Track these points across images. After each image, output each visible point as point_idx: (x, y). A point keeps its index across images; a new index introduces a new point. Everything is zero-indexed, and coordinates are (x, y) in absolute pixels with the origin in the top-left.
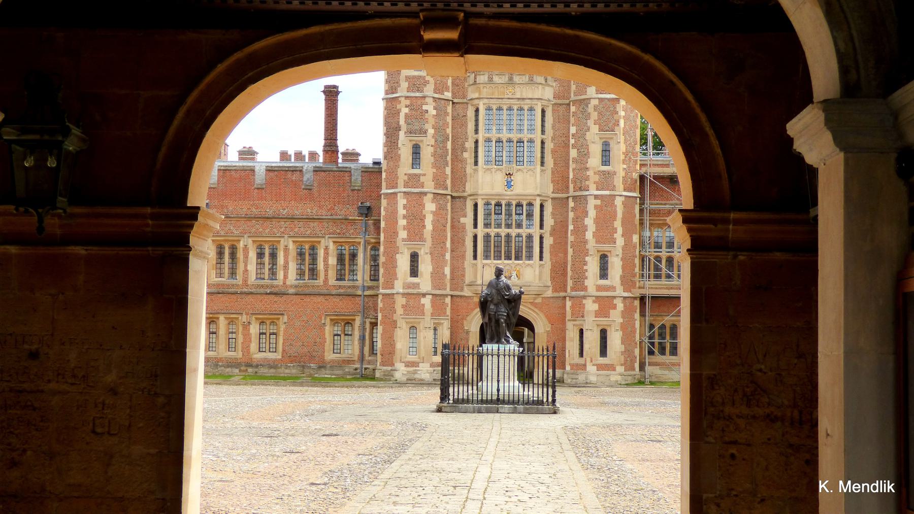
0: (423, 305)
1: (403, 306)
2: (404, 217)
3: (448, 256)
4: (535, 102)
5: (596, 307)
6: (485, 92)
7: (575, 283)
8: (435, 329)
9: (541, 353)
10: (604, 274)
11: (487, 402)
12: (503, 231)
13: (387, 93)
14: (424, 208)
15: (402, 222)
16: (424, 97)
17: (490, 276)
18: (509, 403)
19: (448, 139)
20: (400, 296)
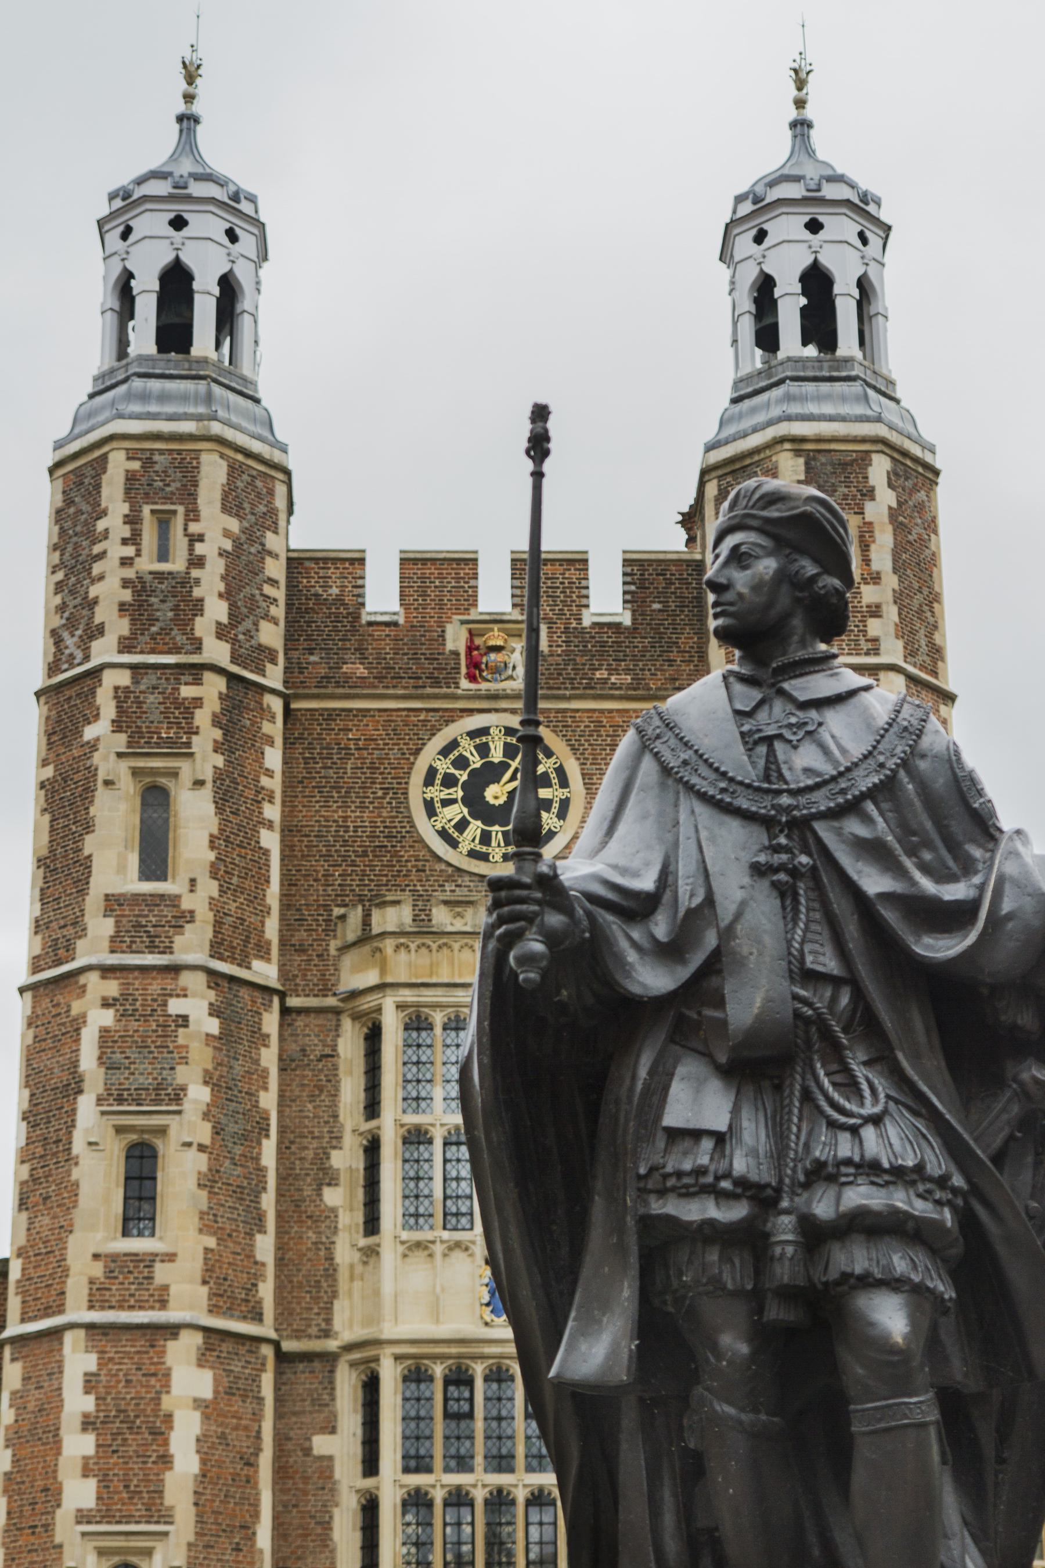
2: (87, 1424)
6: (403, 965)
12: (480, 1482)
13: (36, 966)
14: (166, 1387)
15: (78, 1445)
16: (175, 969)
19: (265, 1132)
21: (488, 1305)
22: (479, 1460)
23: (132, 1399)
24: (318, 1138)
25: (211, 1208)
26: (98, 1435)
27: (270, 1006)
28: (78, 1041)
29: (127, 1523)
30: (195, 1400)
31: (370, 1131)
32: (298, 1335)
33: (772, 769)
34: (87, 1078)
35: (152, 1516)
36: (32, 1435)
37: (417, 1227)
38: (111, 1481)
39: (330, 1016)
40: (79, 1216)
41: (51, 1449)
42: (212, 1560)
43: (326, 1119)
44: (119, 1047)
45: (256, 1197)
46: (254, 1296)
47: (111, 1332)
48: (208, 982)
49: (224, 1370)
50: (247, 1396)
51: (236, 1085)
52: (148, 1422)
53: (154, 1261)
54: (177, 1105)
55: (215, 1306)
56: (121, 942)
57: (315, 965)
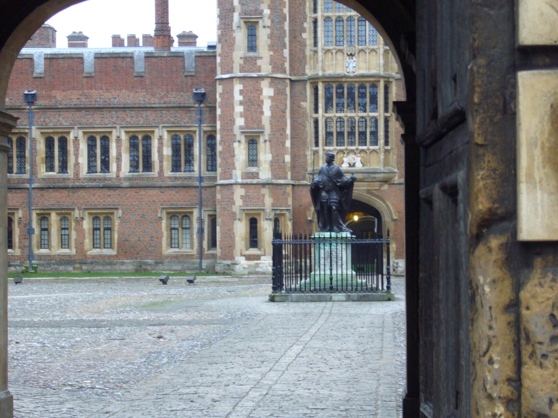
1: (242, 197)
2: (241, 103)
3: (288, 144)
15: (239, 109)
19: (285, 20)
32: (295, 75)
34: (236, 8)
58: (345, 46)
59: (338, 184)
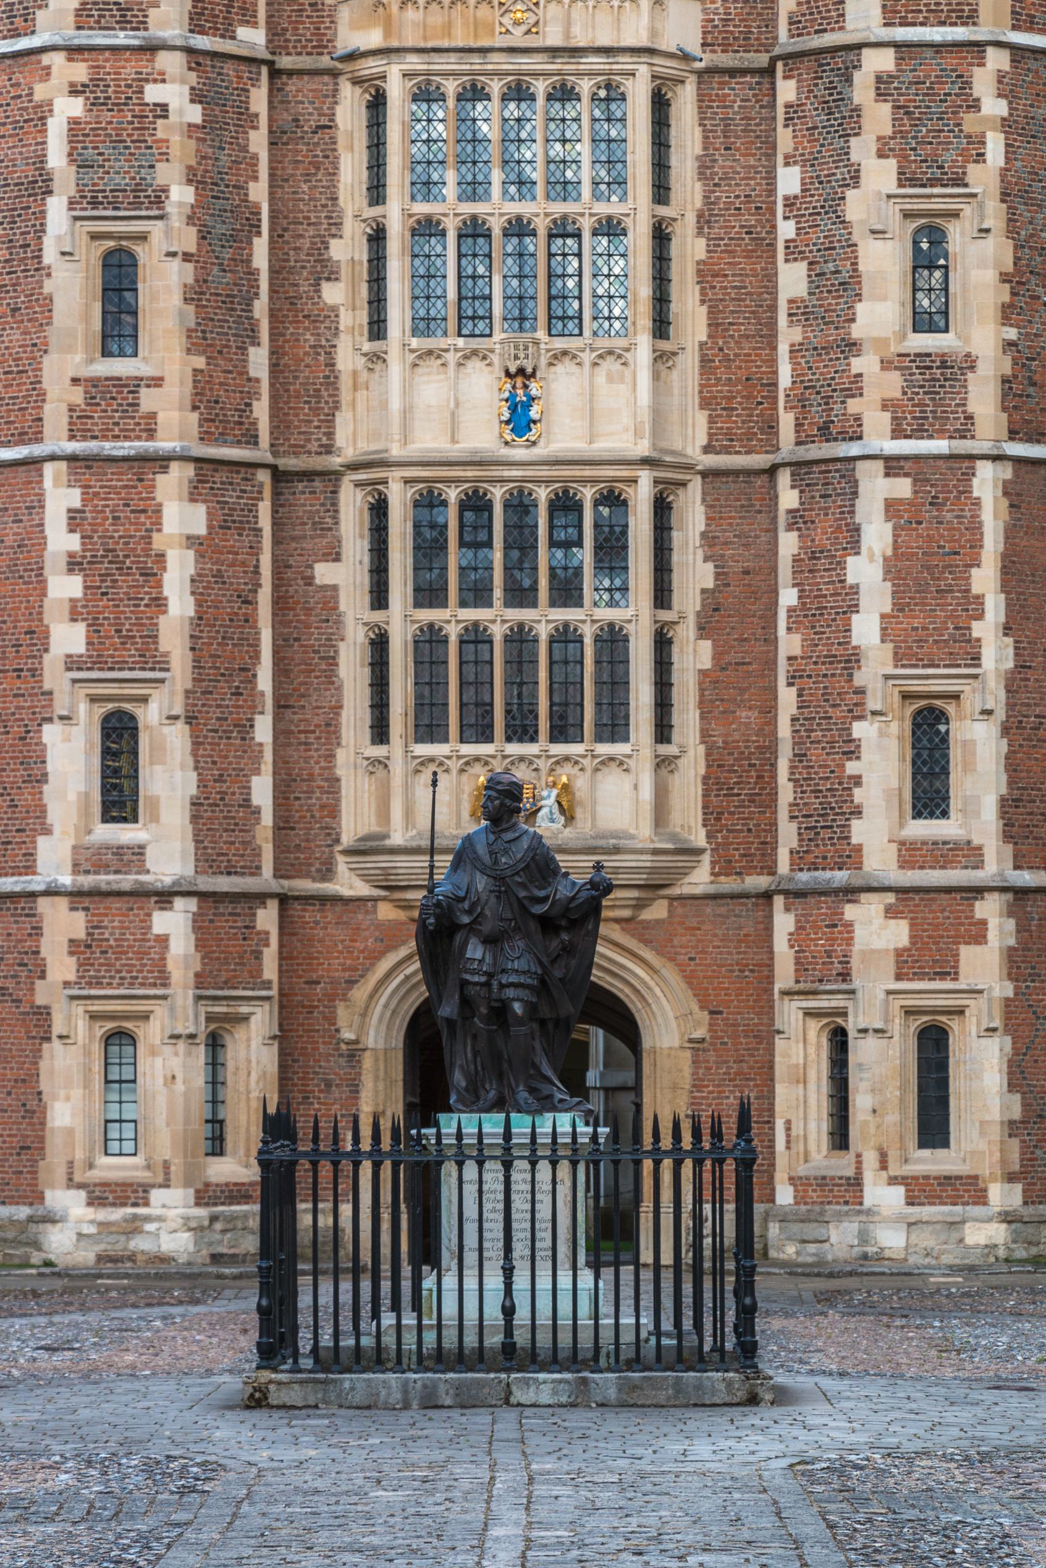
0: (163, 941)
1: (74, 945)
2: (74, 564)
3: (263, 730)
4: (625, 62)
5: (899, 933)
7: (809, 834)
8: (215, 1043)
9: (666, 1143)
10: (930, 793)
11: (460, 1360)
16: (151, 49)
17: (457, 816)
18: (554, 1362)
20: (63, 903)
21: (508, 422)
22: (498, 593)
23: (120, 537)
24: (314, 224)
25: (199, 324)
26: (85, 576)
27: (258, 80)
28: (44, 131)
29: (120, 669)
30: (188, 538)
31: (374, 219)
33: (496, 862)
35: (146, 663)
36: (12, 572)
37: (427, 333)
38: (102, 625)
39: (326, 78)
40: (53, 334)
41: (35, 589)
42: (210, 706)
43: (323, 202)
44: (91, 142)
45: (248, 305)
46: (248, 417)
47: (95, 464)
48: (189, 62)
49: (218, 502)
50: (244, 529)
51: (222, 179)
52: (139, 562)
53: (139, 386)
54: (159, 208)
55: (206, 432)
56: (88, 16)
57: (308, 17)
58: (498, 336)
59: (539, 909)
